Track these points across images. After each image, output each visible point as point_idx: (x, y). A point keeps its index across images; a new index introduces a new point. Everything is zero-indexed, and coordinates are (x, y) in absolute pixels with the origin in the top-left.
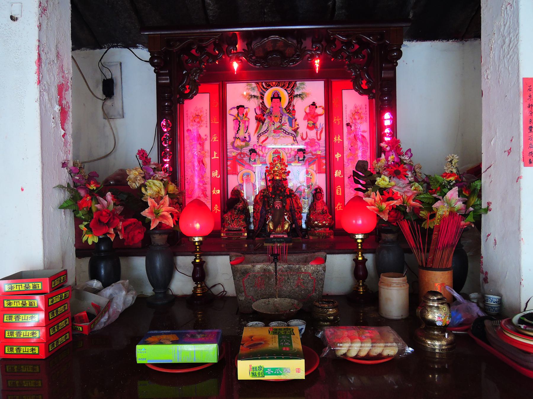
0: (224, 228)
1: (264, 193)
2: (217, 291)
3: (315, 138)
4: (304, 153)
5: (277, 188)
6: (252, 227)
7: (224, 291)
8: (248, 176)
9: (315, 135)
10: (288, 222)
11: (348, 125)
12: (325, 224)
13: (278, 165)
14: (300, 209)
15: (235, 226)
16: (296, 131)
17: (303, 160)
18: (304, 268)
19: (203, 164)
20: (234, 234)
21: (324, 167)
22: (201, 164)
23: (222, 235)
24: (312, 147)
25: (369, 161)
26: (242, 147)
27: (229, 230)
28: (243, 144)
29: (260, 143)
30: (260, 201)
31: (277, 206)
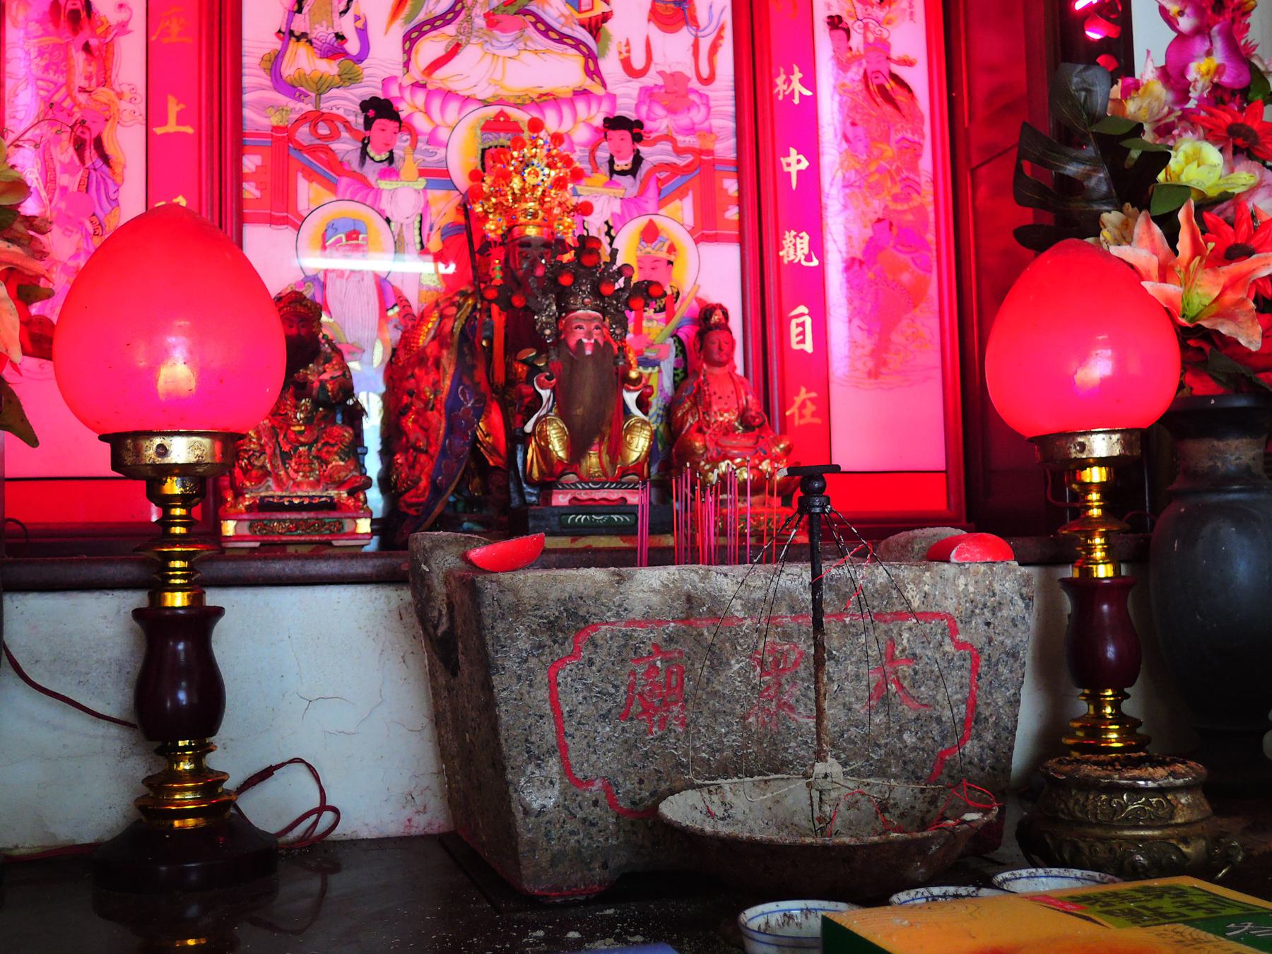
2: (271, 810)
3: (690, 72)
4: (637, 138)
7: (323, 807)
9: (689, 60)
11: (835, 23)
16: (595, 26)
17: (633, 171)
18: (917, 581)
19: (105, 158)
20: (297, 524)
21: (732, 213)
22: (91, 155)
23: (229, 528)
24: (671, 111)
25: (911, 204)
26: (321, 86)
27: (265, 506)
28: (329, 68)
29: (416, 73)
31: (579, 335)
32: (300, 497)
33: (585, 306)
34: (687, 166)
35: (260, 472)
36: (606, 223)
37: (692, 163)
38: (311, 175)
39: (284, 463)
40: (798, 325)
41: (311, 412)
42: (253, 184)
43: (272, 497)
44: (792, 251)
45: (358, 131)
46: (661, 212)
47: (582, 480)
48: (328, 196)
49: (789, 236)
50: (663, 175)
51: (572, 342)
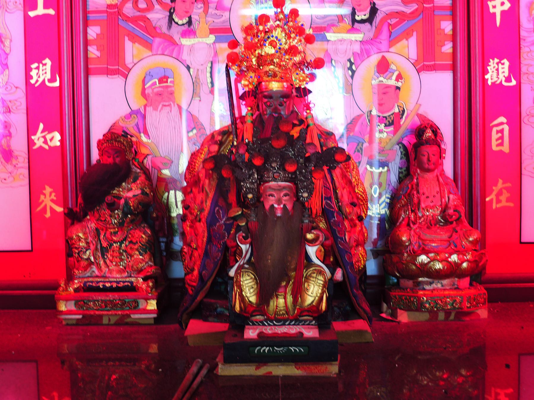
0: (70, 278)
1: (221, 144)
5: (272, 134)
6: (178, 270)
8: (163, 79)
10: (321, 272)
12: (458, 265)
13: (278, 33)
14: (360, 202)
15: (113, 272)
20: (106, 303)
21: (448, 48)
23: (63, 307)
30: (208, 176)
32: (110, 282)
33: (275, 179)
34: (412, 13)
35: (86, 263)
36: (349, 60)
37: (416, 10)
38: (134, 38)
39: (103, 255)
40: (498, 132)
41: (122, 218)
42: (95, 47)
43: (92, 282)
44: (495, 74)
45: (166, 4)
46: (392, 49)
47: (269, 319)
48: (146, 52)
49: (493, 64)
50: (393, 21)
51: (267, 207)
